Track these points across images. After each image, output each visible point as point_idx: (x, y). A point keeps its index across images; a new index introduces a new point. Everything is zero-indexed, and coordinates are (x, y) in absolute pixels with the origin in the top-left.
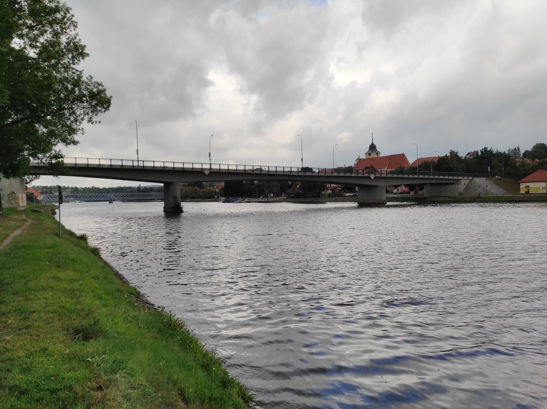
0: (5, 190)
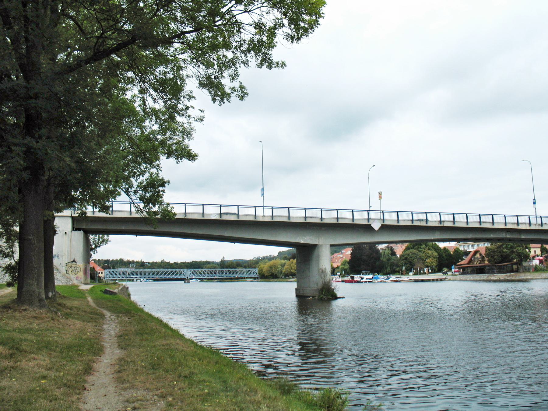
0: (62, 256)
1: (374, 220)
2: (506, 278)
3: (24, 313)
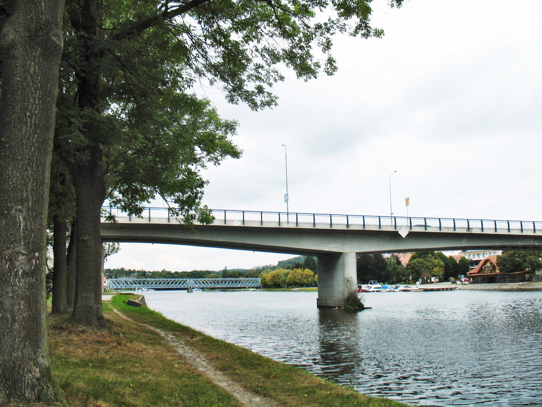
1: (401, 226)
2: (519, 287)
3: (84, 336)
